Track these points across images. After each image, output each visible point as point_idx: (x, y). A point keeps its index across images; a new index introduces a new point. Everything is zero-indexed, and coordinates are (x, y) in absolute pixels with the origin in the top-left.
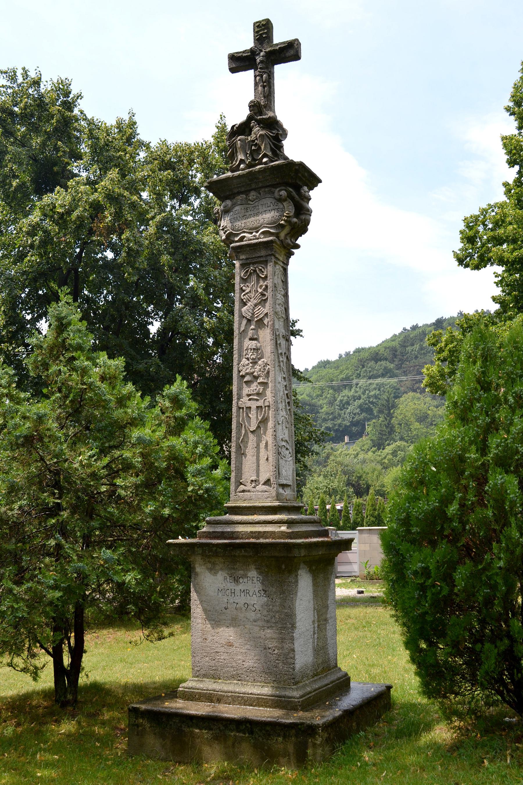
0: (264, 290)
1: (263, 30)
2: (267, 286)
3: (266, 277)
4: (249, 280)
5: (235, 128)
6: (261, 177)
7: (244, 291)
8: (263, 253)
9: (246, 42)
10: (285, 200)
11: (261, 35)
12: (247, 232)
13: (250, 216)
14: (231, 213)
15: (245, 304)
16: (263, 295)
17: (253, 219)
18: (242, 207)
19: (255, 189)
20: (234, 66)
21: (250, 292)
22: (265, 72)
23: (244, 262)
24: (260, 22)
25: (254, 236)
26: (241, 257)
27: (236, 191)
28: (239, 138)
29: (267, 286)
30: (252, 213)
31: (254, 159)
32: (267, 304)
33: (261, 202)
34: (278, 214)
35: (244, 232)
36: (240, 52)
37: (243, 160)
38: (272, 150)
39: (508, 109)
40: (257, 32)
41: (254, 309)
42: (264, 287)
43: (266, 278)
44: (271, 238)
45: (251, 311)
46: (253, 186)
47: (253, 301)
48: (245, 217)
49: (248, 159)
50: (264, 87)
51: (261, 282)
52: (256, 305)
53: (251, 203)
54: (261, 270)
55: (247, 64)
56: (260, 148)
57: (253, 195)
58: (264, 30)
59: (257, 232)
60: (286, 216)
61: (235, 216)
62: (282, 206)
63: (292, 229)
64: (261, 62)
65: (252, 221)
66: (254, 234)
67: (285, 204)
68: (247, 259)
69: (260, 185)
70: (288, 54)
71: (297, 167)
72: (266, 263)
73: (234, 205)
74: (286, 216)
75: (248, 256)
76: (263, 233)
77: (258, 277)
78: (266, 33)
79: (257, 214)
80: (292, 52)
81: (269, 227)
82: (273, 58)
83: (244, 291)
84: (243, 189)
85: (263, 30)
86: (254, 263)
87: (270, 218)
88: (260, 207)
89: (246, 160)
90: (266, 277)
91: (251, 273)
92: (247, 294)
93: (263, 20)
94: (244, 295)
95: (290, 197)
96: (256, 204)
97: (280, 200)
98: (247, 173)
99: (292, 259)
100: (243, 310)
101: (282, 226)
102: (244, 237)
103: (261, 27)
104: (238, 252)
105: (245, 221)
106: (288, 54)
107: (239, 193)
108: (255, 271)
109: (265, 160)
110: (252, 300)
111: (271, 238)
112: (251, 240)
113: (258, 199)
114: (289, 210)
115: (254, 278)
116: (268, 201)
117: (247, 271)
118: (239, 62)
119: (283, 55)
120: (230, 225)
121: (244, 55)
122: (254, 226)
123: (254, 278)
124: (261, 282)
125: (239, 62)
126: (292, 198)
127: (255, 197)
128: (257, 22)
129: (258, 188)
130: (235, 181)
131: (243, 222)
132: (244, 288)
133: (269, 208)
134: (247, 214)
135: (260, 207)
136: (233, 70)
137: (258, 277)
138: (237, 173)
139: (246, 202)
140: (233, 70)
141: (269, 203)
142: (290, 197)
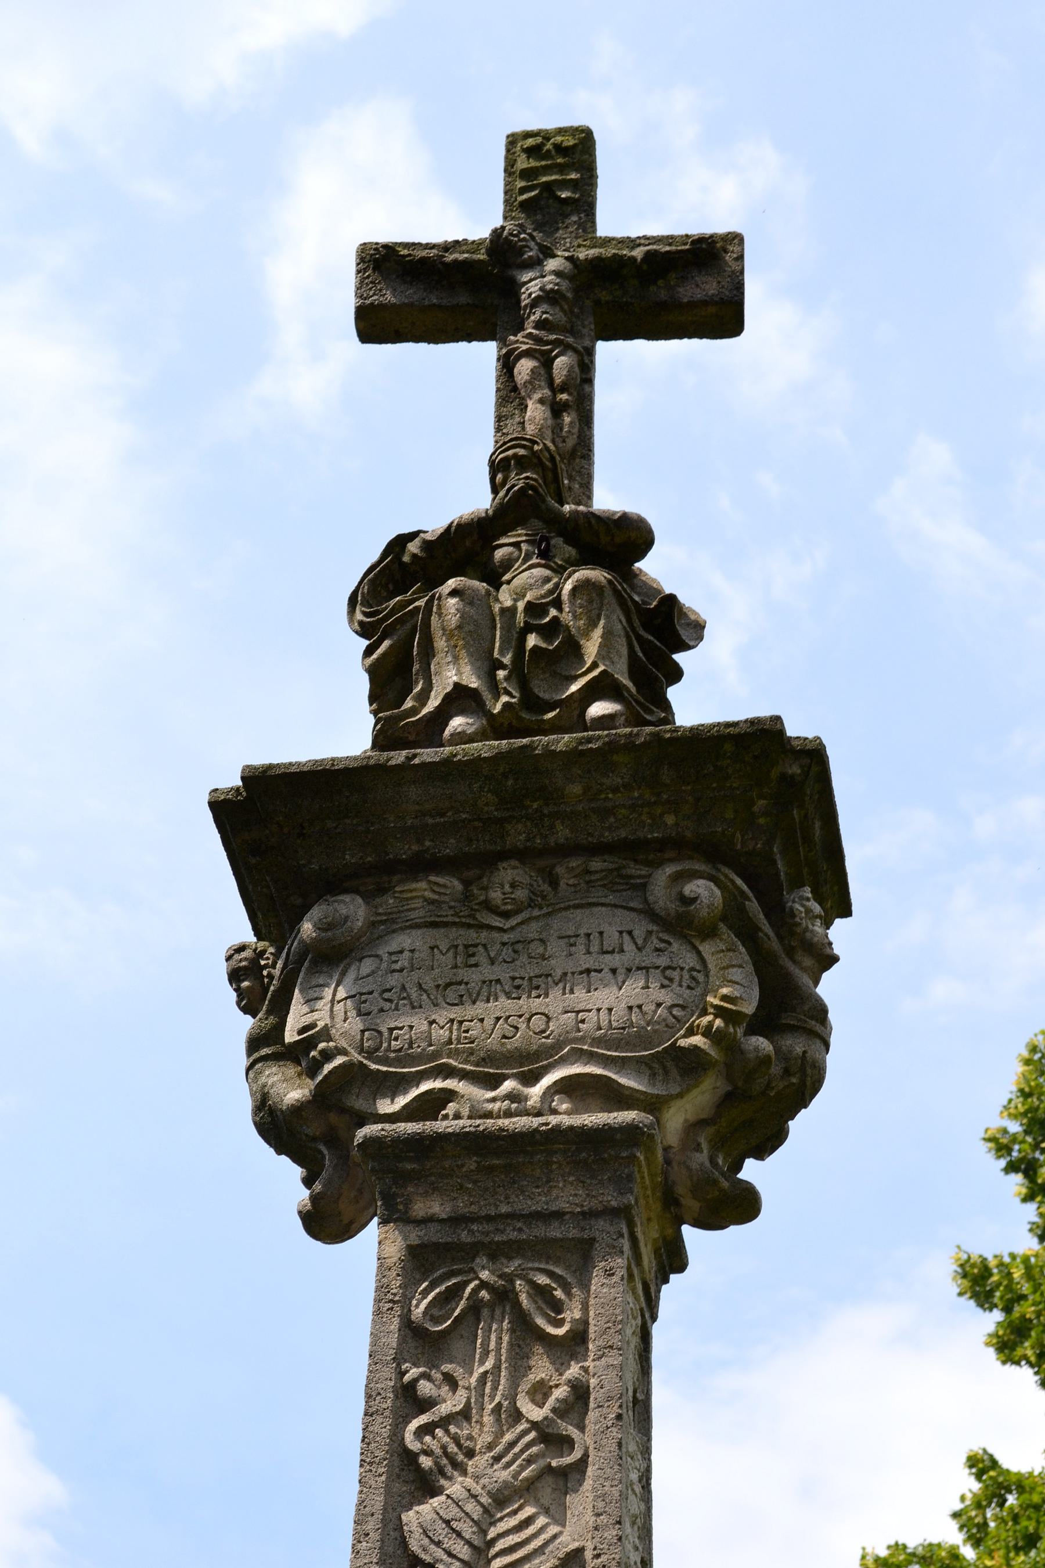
0: (562, 1411)
1: (554, 171)
2: (580, 1393)
3: (578, 1338)
4: (458, 1346)
5: (413, 547)
6: (576, 789)
7: (425, 1405)
8: (567, 1195)
9: (464, 211)
10: (709, 933)
11: (548, 187)
12: (464, 1075)
13: (489, 990)
14: (367, 966)
15: (426, 1486)
16: (550, 1438)
17: (503, 1005)
18: (442, 938)
19: (522, 855)
20: (389, 297)
21: (465, 1414)
22: (566, 348)
23: (433, 1234)
24: (545, 135)
25: (512, 1097)
26: (420, 1208)
27: (404, 850)
28: (452, 583)
29: (580, 1393)
30: (503, 972)
31: (531, 702)
32: (581, 1503)
33: (559, 924)
34: (666, 997)
35: (447, 1072)
36: (433, 246)
37: (474, 693)
38: (635, 670)
39: (1000, 1145)
40: (526, 174)
41: (489, 1516)
42: (560, 1393)
43: (576, 1342)
44: (629, 1116)
45: (468, 1530)
46: (517, 835)
47: (485, 1473)
48: (454, 991)
49: (496, 691)
50: (557, 410)
51: (541, 1368)
52: (502, 1498)
53: (497, 922)
54: (541, 1293)
55: (463, 299)
56: (573, 649)
57: (508, 881)
58: (562, 169)
59: (531, 1078)
60: (720, 1012)
61: (393, 980)
62: (689, 960)
63: (728, 1099)
64: (549, 297)
65: (493, 1019)
66: (508, 1085)
67: (706, 948)
68: (456, 1221)
69: (562, 833)
70: (688, 292)
71: (795, 769)
72: (581, 1256)
73: (383, 926)
74: (720, 1012)
75: (462, 1206)
76: (567, 1087)
77: (526, 1333)
78: (574, 185)
79: (538, 984)
80: (708, 287)
81: (606, 1061)
82: (604, 296)
83: (425, 1405)
84: (450, 847)
85: (554, 171)
86: (496, 1253)
87: (620, 1010)
88: (555, 947)
89: (487, 696)
90: (578, 1338)
91: (475, 1309)
92: (444, 1422)
93: (561, 131)
94: (426, 1430)
95: (735, 919)
96: (532, 930)
97: (682, 925)
98: (499, 757)
99: (674, 1293)
100: (409, 1517)
101: (687, 1065)
102: (449, 1095)
103: (547, 155)
104: (403, 1178)
105: (455, 1013)
106: (688, 292)
107: (421, 866)
108: (504, 1296)
109: (598, 709)
110: (480, 1462)
111: (629, 1116)
112: (489, 1115)
113: (543, 903)
114: (735, 987)
115: (497, 1337)
116: (609, 923)
117: (452, 1295)
118: (411, 294)
119: (659, 292)
120: (355, 1024)
121: (450, 257)
122: (511, 1045)
123: (497, 1337)
124: (541, 1368)
125: (411, 294)
126: (748, 935)
127: (521, 894)
128: (528, 135)
129: (542, 853)
130: (413, 792)
131: (442, 1016)
132: (425, 1388)
133: (615, 960)
134: (474, 976)
135: (555, 947)
136: (375, 325)
137: (526, 1333)
138: (427, 755)
139: (470, 914)
140: (375, 325)
141: (612, 937)
142: (735, 919)
